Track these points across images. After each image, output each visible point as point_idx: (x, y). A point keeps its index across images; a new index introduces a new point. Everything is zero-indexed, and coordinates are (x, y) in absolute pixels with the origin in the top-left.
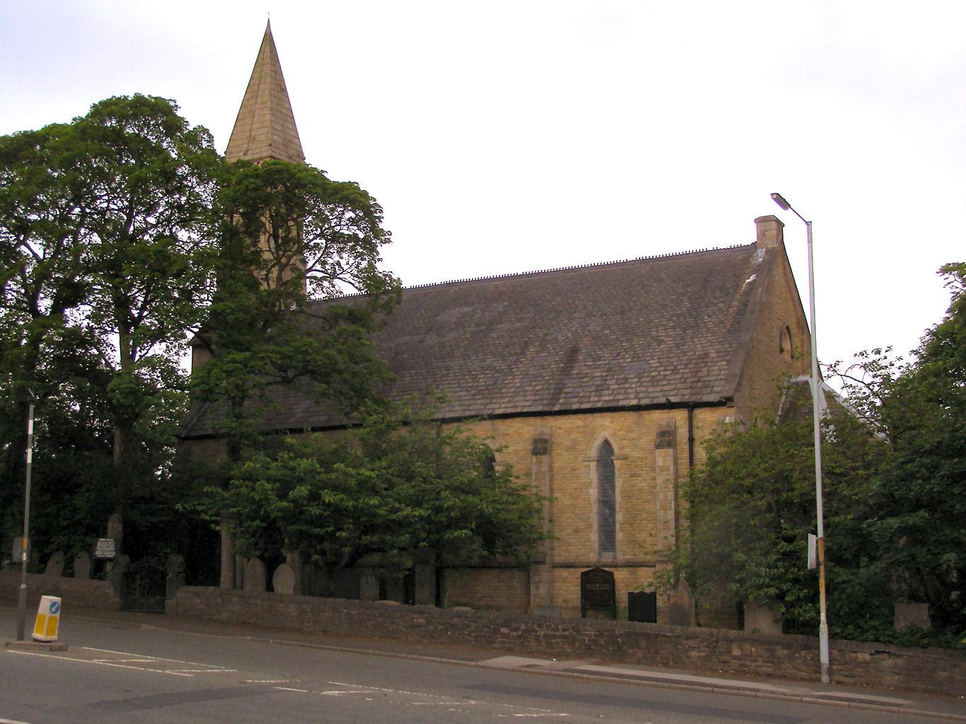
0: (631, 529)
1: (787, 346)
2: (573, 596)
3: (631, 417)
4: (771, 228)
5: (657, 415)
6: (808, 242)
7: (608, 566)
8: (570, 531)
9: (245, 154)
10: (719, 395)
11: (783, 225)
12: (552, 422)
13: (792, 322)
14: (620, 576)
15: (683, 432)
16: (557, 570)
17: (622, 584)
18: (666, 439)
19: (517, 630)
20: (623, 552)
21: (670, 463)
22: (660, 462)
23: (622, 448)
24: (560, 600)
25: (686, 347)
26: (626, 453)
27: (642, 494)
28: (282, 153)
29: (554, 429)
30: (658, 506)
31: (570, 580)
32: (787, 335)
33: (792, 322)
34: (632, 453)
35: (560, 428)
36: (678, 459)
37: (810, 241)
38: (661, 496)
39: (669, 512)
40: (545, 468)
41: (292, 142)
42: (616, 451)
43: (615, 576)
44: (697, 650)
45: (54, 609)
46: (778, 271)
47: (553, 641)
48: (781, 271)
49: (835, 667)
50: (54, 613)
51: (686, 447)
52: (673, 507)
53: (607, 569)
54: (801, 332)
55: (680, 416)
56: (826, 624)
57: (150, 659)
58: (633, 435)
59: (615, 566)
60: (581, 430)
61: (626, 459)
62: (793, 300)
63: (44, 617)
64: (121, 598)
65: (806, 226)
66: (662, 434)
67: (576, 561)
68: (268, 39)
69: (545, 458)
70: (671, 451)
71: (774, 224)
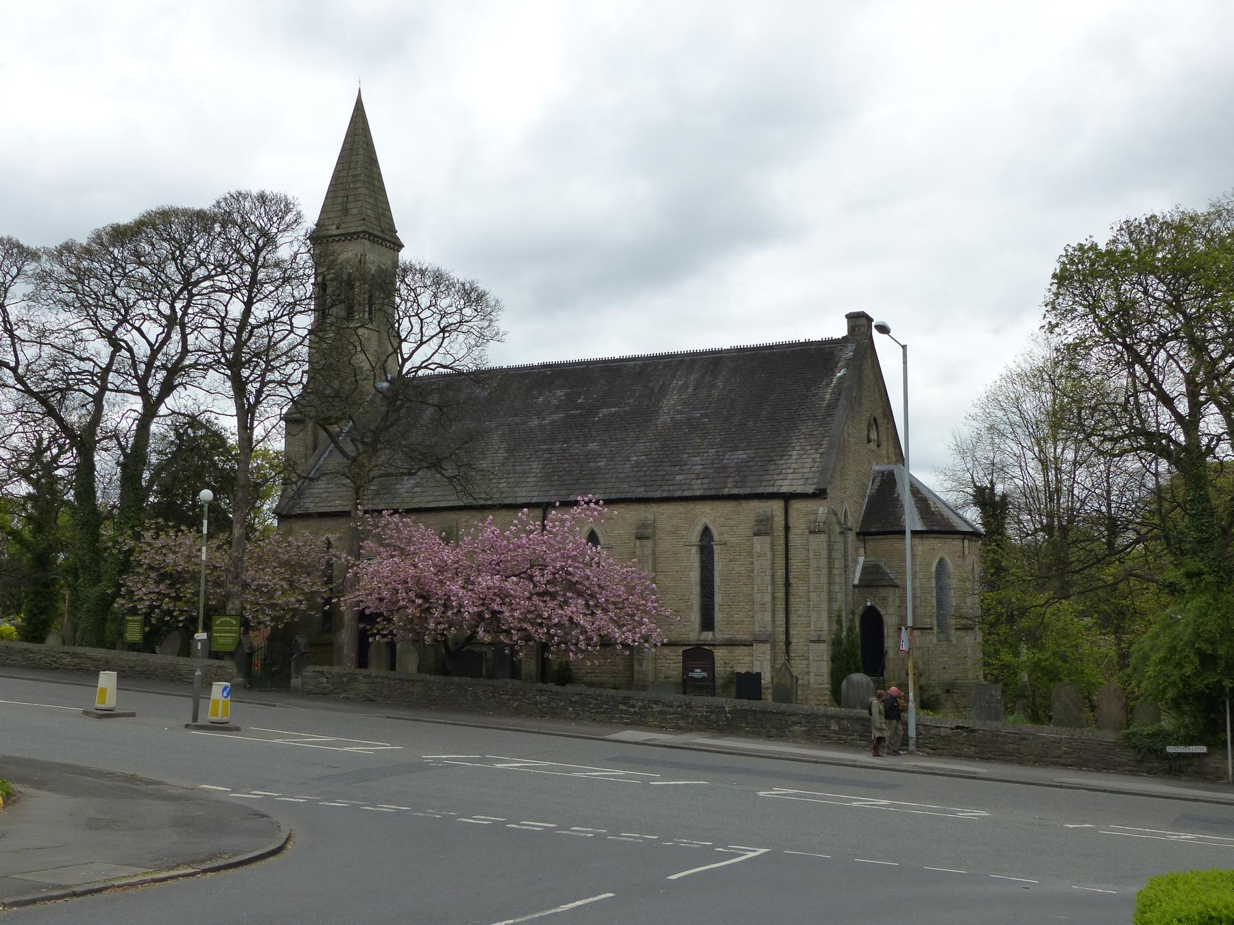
1: (874, 436)
2: (675, 673)
3: (729, 507)
4: (860, 323)
5: (755, 505)
7: (706, 645)
9: (338, 228)
10: (814, 486)
12: (656, 509)
14: (719, 654)
17: (721, 662)
18: (763, 527)
19: (634, 706)
20: (721, 631)
21: (767, 548)
22: (757, 548)
23: (721, 534)
24: (662, 676)
25: (781, 438)
28: (375, 227)
30: (756, 590)
31: (672, 658)
33: (878, 413)
35: (663, 514)
37: (905, 363)
38: (758, 580)
39: (765, 595)
40: (648, 551)
41: (383, 215)
42: (716, 537)
43: (715, 654)
45: (225, 694)
46: (867, 366)
47: (668, 717)
48: (870, 365)
49: (920, 741)
50: (226, 697)
51: (783, 534)
52: (769, 591)
53: (707, 648)
54: (886, 421)
55: (777, 506)
57: (621, 773)
58: (732, 523)
59: (714, 645)
61: (725, 544)
62: (880, 392)
63: (218, 701)
68: (359, 109)
69: (649, 543)
70: (768, 538)
71: (864, 321)
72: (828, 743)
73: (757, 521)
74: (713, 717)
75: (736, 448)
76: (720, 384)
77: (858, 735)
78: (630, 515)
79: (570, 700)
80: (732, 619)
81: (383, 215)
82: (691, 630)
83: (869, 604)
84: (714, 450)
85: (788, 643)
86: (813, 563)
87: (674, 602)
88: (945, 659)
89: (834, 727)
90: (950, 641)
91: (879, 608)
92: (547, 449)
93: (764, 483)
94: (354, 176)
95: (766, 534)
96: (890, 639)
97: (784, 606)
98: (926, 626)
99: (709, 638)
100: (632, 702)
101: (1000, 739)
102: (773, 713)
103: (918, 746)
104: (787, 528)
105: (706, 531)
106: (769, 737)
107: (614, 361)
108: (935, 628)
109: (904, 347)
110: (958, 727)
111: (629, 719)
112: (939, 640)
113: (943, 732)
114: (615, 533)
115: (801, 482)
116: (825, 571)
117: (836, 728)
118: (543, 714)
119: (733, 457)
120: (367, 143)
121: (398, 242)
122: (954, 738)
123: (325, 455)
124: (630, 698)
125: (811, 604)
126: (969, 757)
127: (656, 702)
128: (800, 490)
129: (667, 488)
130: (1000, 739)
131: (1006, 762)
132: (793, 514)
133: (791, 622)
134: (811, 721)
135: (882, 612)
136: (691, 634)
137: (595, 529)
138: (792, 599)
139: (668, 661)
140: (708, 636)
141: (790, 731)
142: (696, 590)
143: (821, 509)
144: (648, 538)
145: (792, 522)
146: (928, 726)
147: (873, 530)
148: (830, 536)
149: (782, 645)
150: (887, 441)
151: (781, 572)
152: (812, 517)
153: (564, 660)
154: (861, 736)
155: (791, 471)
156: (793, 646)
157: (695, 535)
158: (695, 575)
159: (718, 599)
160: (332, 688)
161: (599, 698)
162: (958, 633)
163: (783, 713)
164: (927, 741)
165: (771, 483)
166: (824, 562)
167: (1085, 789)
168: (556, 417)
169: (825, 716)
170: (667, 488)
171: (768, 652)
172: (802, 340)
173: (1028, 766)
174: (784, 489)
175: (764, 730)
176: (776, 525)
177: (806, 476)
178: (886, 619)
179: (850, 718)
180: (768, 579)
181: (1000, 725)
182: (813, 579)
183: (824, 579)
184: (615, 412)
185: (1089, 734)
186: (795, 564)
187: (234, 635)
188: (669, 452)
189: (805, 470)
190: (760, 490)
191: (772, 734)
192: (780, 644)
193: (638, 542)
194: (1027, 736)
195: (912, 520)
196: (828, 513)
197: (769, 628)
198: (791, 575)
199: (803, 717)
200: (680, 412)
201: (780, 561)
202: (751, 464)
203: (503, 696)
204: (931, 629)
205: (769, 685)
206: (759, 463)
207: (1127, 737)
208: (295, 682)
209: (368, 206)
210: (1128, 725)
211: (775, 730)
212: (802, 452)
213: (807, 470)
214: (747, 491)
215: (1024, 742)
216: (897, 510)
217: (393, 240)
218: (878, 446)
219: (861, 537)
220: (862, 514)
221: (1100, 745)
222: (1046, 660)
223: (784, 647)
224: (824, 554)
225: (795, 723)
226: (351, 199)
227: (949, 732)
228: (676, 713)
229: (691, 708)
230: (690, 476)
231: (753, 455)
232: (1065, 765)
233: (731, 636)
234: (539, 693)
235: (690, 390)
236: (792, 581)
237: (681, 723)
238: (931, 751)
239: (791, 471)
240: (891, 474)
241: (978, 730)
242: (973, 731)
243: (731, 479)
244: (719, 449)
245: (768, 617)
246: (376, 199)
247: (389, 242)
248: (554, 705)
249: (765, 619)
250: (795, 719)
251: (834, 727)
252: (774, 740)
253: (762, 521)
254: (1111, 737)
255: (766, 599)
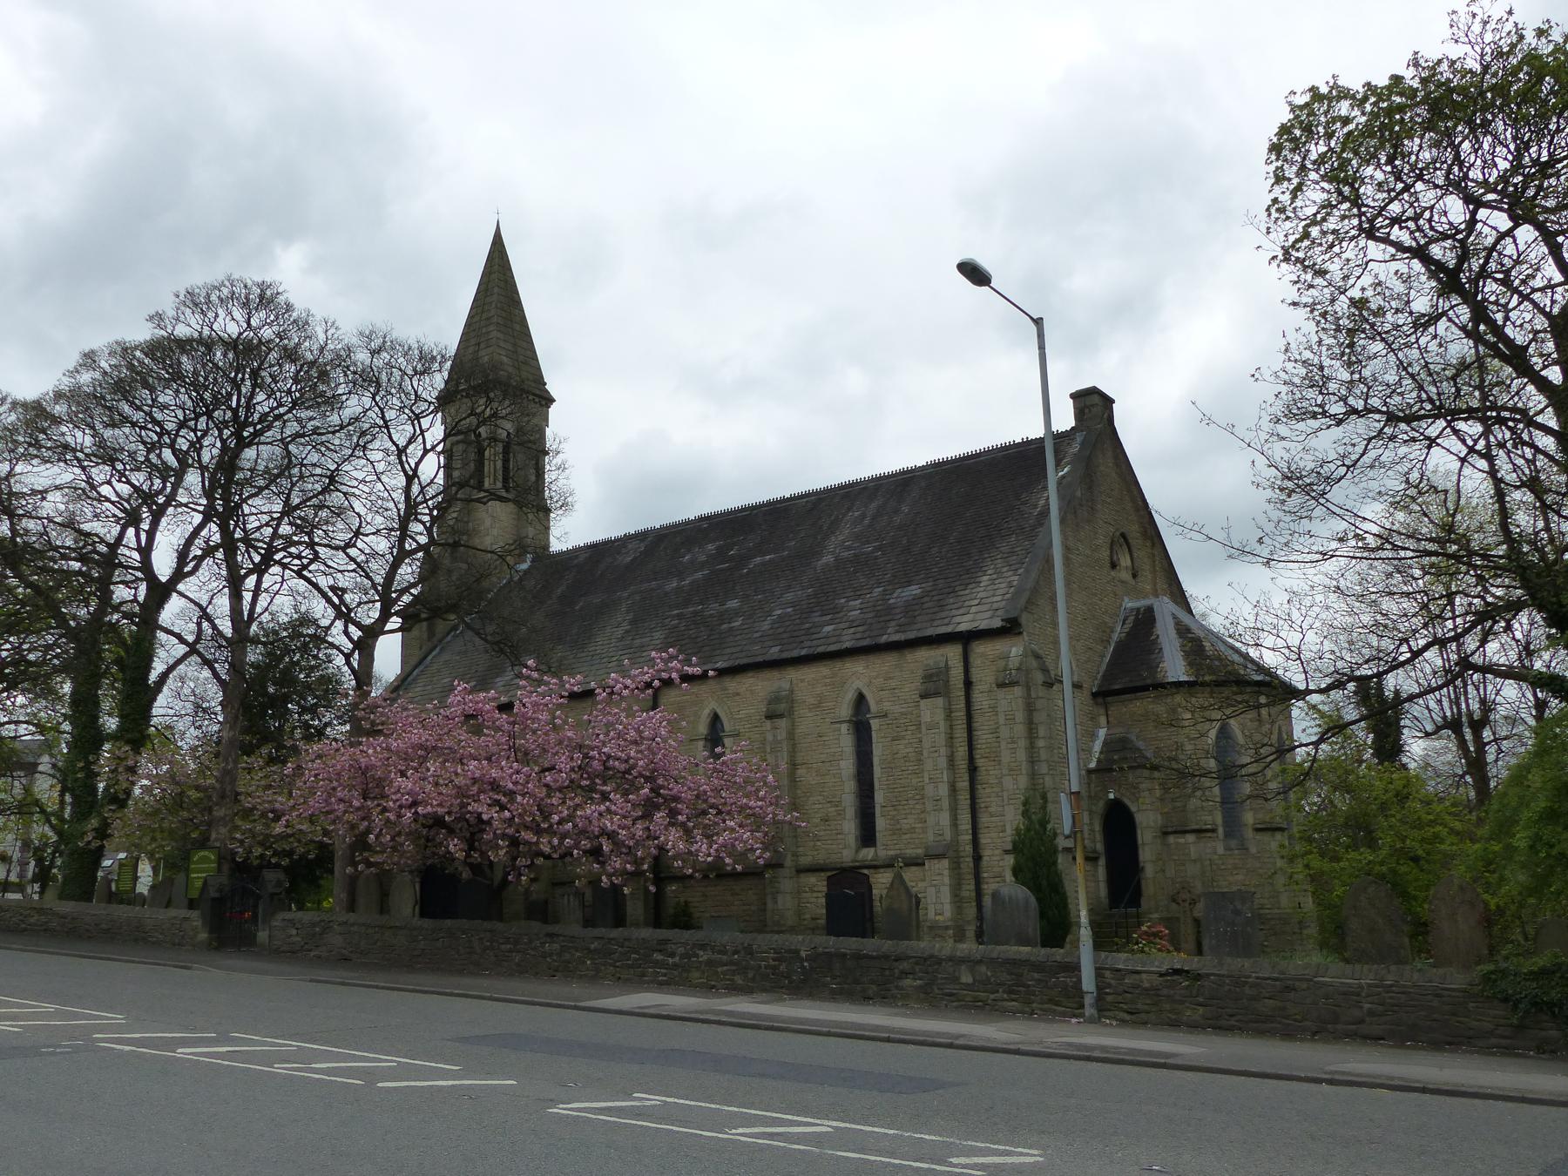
0: (895, 813)
6: (1039, 348)
8: (817, 821)
11: (1113, 401)
12: (793, 674)
13: (1133, 530)
15: (957, 673)
16: (802, 875)
18: (934, 685)
19: (672, 955)
21: (940, 716)
22: (926, 717)
23: (879, 702)
24: (807, 916)
26: (885, 708)
27: (907, 764)
29: (795, 682)
30: (927, 780)
32: (1125, 547)
33: (1133, 530)
34: (892, 708)
35: (802, 681)
36: (951, 712)
37: (1042, 347)
38: (929, 765)
41: (525, 363)
44: (911, 976)
46: (1105, 464)
47: (719, 970)
55: (953, 653)
56: (1089, 928)
58: (893, 683)
59: (875, 867)
60: (828, 680)
61: (885, 716)
64: (211, 932)
65: (1034, 328)
66: (928, 677)
67: (827, 861)
69: (783, 723)
70: (940, 701)
72: (956, 1007)
73: (925, 677)
74: (783, 968)
75: (909, 583)
76: (905, 509)
77: (1004, 992)
78: (758, 687)
79: (588, 949)
80: (898, 827)
81: (525, 363)
82: (843, 846)
83: (1111, 796)
84: (881, 589)
85: (977, 858)
86: (1005, 732)
87: (820, 806)
88: (1240, 877)
89: (966, 978)
90: (1247, 849)
91: (1126, 801)
92: (678, 615)
93: (935, 623)
94: (488, 319)
95: (936, 694)
96: (1146, 848)
97: (969, 802)
98: (1204, 827)
99: (870, 857)
100: (670, 947)
101: (1247, 990)
102: (872, 958)
103: (1102, 1008)
104: (968, 684)
105: (861, 699)
106: (866, 999)
107: (784, 500)
108: (1221, 830)
109: (1038, 322)
110: (1177, 972)
111: (665, 975)
112: (1227, 848)
113: (1146, 981)
114: (742, 714)
115: (989, 614)
116: (1022, 743)
117: (970, 980)
118: (552, 973)
119: (903, 594)
120: (506, 281)
121: (546, 395)
122: (1165, 991)
123: (434, 653)
124: (666, 941)
125: (1005, 794)
126: (1194, 1027)
127: (703, 947)
128: (984, 625)
129: (809, 643)
130: (1247, 990)
131: (1261, 1033)
132: (976, 661)
133: (980, 826)
134: (930, 969)
135: (1133, 808)
136: (845, 852)
137: (718, 711)
138: (982, 792)
139: (815, 895)
140: (868, 854)
141: (897, 987)
142: (850, 786)
143: (1014, 650)
144: (781, 716)
145: (976, 674)
146: (1118, 970)
147: (1117, 687)
148: (1028, 689)
149: (967, 864)
150: (1154, 572)
151: (962, 751)
152: (1002, 663)
153: (682, 900)
154: (1011, 992)
155: (976, 602)
156: (985, 862)
157: (846, 706)
158: (848, 766)
159: (879, 797)
160: (302, 943)
161: (627, 943)
162: (1259, 836)
163: (886, 957)
164: (1120, 999)
165: (946, 621)
166: (1020, 729)
167: (1331, 1082)
168: (699, 575)
169: (951, 959)
170: (809, 643)
171: (946, 872)
172: (1018, 440)
173: (1302, 1040)
174: (963, 627)
175: (859, 987)
176: (953, 681)
177: (995, 606)
178: (1139, 818)
179: (992, 962)
180: (943, 762)
181: (1247, 963)
182: (1006, 758)
183: (1022, 755)
184: (770, 560)
185: (1417, 974)
186: (983, 737)
187: (195, 875)
188: (823, 599)
189: (995, 599)
190: (930, 632)
191: (870, 993)
192: (967, 859)
193: (768, 724)
194: (1297, 984)
195: (1175, 667)
196: (1025, 655)
197: (948, 835)
198: (977, 754)
199: (917, 964)
200: (849, 548)
201: (961, 733)
202: (923, 601)
203: (503, 947)
204: (1213, 831)
205: (949, 923)
206: (936, 598)
207: (1486, 978)
208: (262, 936)
209: (503, 353)
210: (1492, 950)
211: (874, 987)
212: (995, 576)
213: (999, 598)
214: (911, 635)
215: (1292, 995)
216: (1155, 656)
217: (538, 392)
218: (1134, 576)
219: (1100, 700)
220: (1104, 667)
221: (1437, 996)
222: (1382, 863)
223: (972, 865)
224: (1020, 716)
225: (905, 974)
226: (482, 346)
227: (1157, 980)
228: (732, 963)
229: (751, 954)
230: (841, 626)
231: (929, 589)
232: (1376, 1039)
233: (899, 852)
234: (548, 940)
235: (866, 522)
236: (980, 762)
237: (739, 980)
238: (1127, 1017)
239: (976, 602)
240: (1150, 610)
241: (1208, 975)
242: (1198, 977)
243: (893, 623)
244: (887, 588)
245: (945, 819)
246: (515, 345)
247: (534, 394)
248: (567, 956)
249: (940, 824)
250: (905, 965)
251: (966, 978)
252: (874, 1005)
253: (931, 676)
254: (1457, 979)
255: (941, 793)
